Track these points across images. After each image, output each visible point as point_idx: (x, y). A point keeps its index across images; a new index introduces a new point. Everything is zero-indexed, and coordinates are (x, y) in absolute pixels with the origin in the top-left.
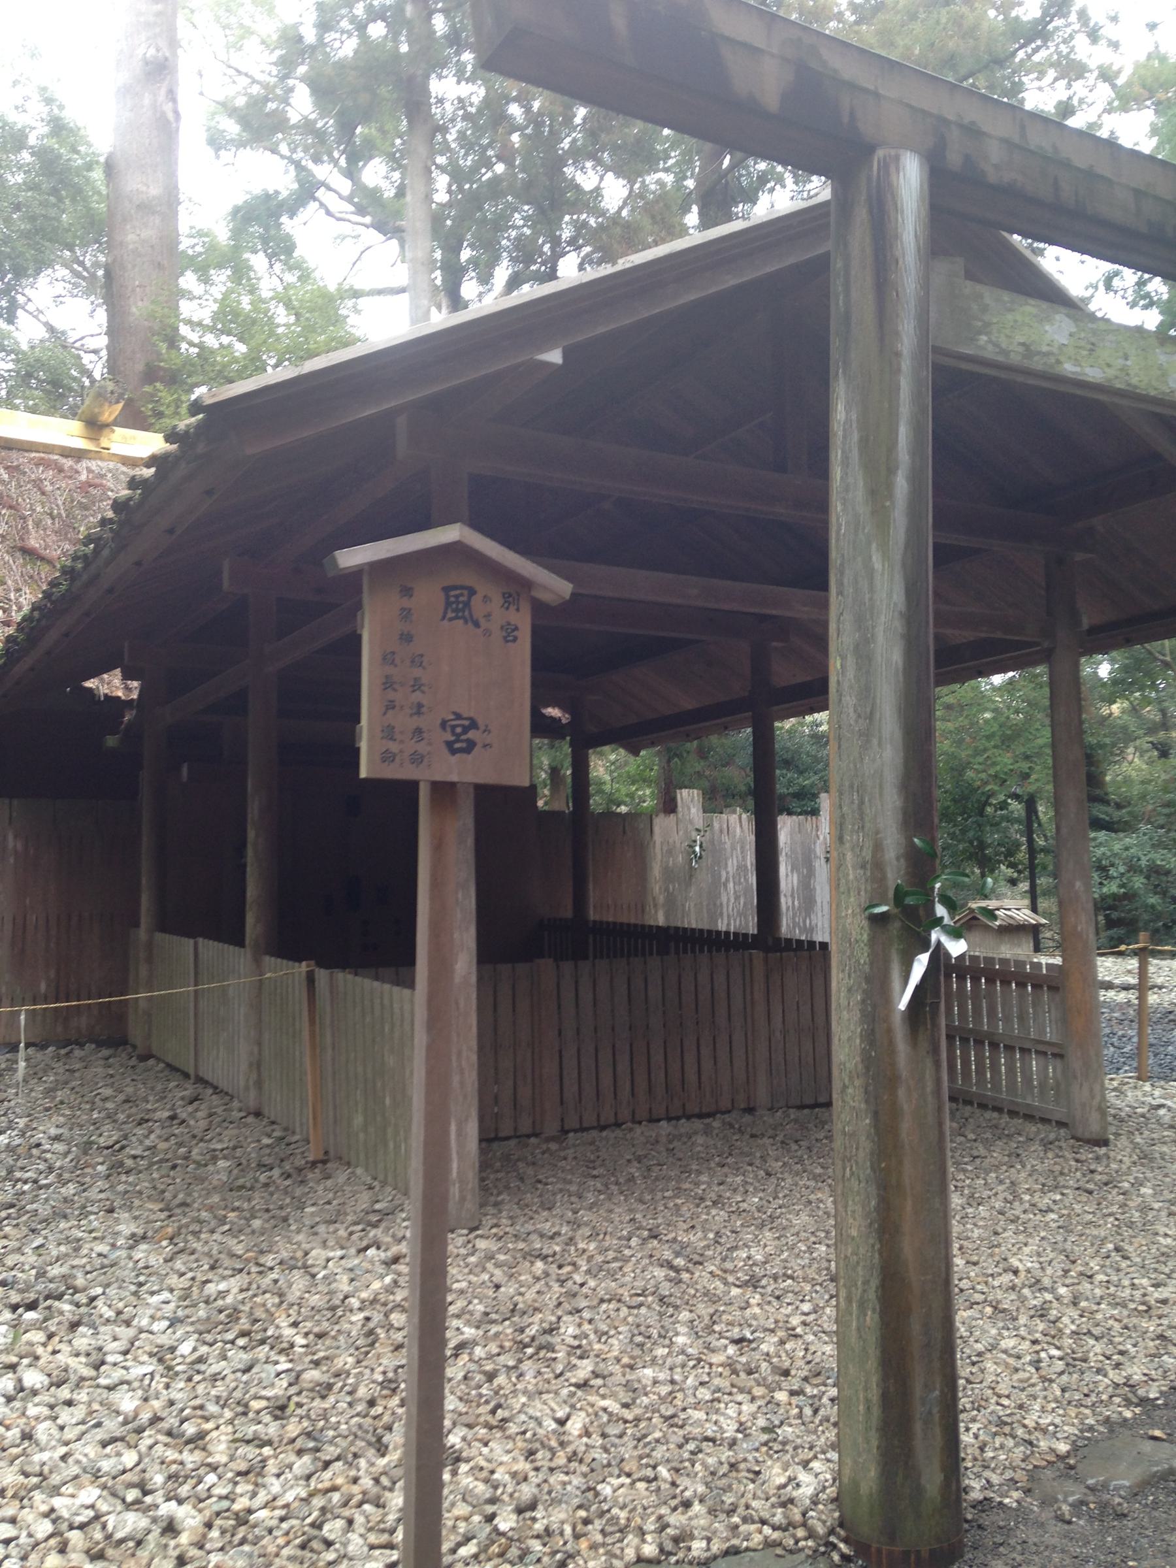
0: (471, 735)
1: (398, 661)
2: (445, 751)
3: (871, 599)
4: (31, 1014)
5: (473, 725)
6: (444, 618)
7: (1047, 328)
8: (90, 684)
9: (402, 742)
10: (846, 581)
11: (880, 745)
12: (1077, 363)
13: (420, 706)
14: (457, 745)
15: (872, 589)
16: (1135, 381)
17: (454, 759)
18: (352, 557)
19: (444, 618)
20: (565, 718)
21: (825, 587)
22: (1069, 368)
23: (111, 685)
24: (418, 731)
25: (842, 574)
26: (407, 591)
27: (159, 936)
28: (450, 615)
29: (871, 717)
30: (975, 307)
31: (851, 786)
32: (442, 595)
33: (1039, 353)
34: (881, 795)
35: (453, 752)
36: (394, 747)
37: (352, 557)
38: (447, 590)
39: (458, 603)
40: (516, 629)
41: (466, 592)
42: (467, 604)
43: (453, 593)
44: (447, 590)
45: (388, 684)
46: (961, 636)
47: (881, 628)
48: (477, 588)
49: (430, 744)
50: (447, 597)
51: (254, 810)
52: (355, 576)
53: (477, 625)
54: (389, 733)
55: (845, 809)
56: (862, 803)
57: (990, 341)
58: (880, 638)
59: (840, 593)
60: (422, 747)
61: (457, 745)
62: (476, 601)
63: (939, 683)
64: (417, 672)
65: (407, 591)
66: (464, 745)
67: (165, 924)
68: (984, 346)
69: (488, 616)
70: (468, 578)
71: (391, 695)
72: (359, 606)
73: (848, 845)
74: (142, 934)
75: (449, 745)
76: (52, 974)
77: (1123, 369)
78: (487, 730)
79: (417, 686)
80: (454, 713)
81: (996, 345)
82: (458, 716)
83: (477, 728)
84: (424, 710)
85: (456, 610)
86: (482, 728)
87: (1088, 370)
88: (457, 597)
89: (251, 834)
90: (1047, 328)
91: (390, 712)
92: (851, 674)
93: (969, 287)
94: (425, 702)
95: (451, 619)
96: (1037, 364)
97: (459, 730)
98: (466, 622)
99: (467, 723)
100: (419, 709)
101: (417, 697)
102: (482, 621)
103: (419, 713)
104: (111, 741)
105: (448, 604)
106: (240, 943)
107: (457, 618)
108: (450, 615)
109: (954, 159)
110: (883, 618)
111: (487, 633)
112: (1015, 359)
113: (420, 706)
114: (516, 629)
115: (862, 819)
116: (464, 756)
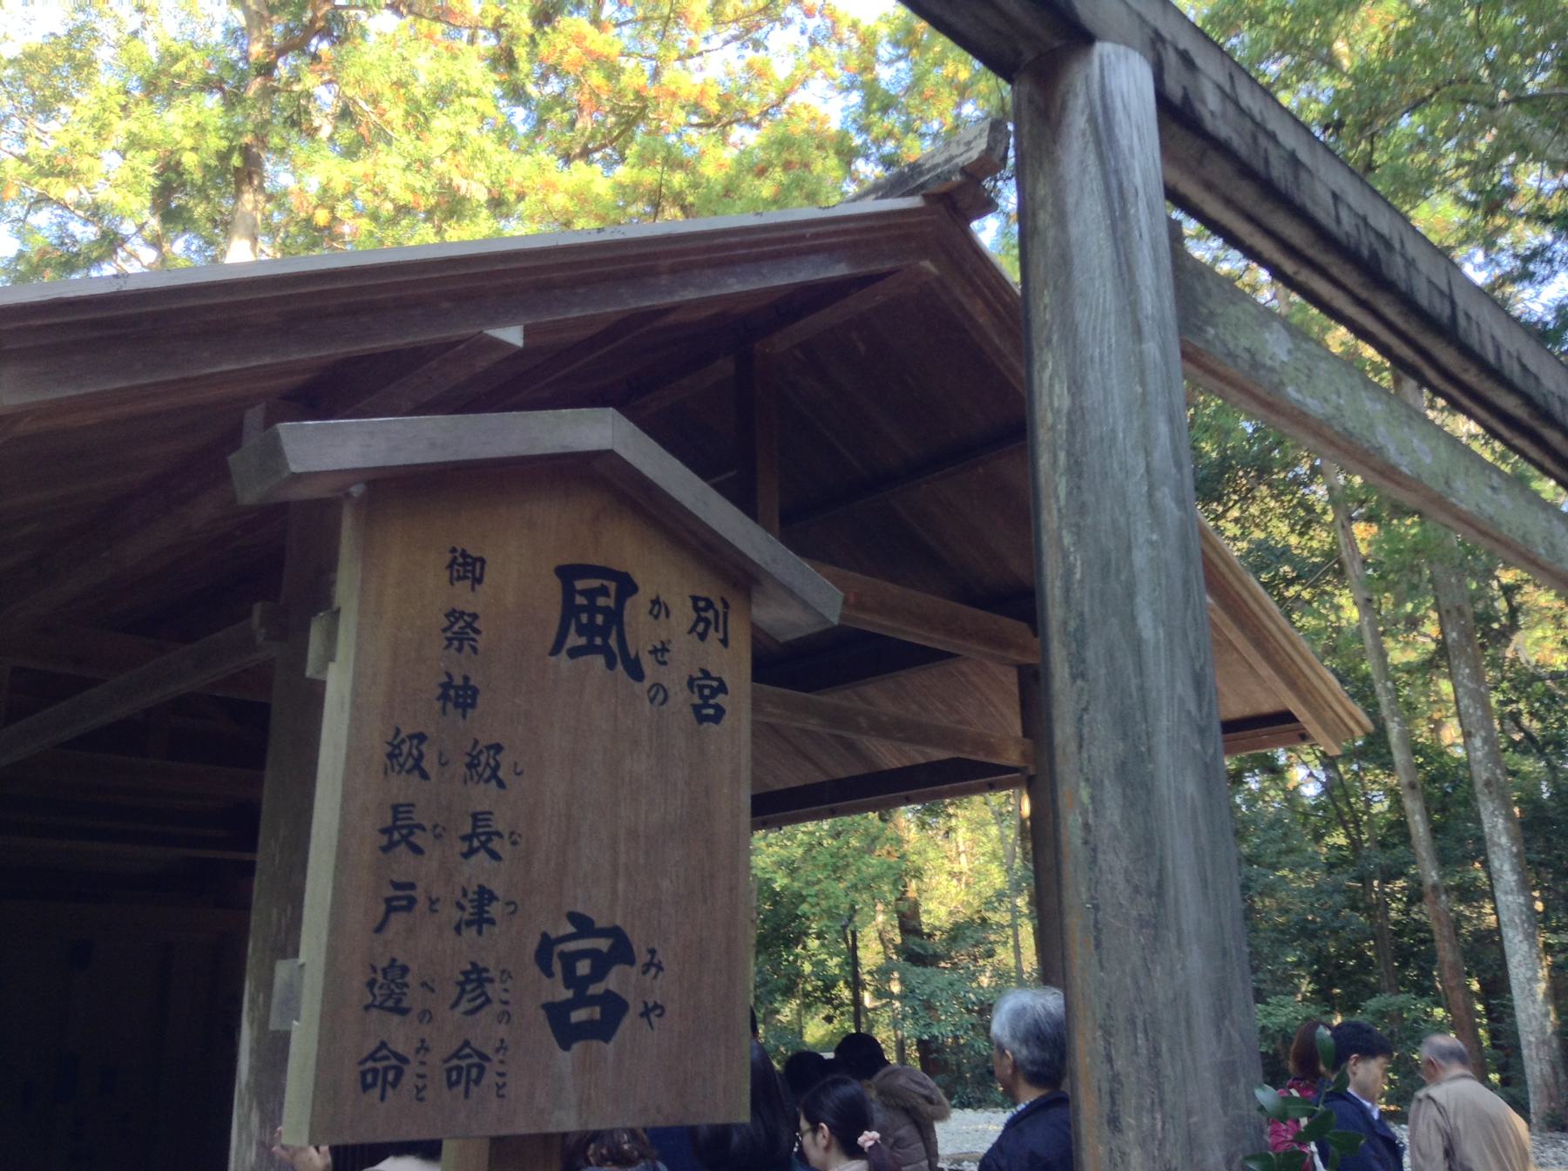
0: (614, 980)
1: (429, 764)
2: (545, 1034)
3: (1141, 688)
5: (622, 950)
6: (556, 650)
7: (1267, 335)
9: (426, 1015)
10: (1090, 655)
11: (1179, 944)
12: (1299, 390)
13: (485, 896)
14: (578, 1016)
15: (1140, 671)
17: (565, 1060)
19: (556, 650)
21: (261, 765)
24: (475, 977)
25: (1082, 643)
28: (574, 640)
29: (1159, 892)
30: (1199, 288)
31: (1132, 1021)
32: (556, 584)
33: (1264, 366)
34: (1190, 1044)
35: (566, 1034)
36: (400, 1035)
38: (568, 574)
39: (592, 609)
40: (722, 688)
41: (612, 586)
42: (615, 617)
43: (580, 585)
44: (568, 574)
45: (400, 830)
46: (790, 777)
47: (1164, 737)
48: (638, 578)
49: (505, 1017)
50: (569, 592)
53: (635, 670)
54: (389, 988)
55: (1119, 1064)
56: (1156, 1053)
57: (1217, 336)
58: (1164, 756)
59: (1078, 674)
60: (485, 1031)
61: (578, 1016)
62: (636, 611)
63: (756, 826)
64: (482, 796)
66: (596, 1012)
69: (660, 651)
70: (625, 547)
71: (404, 865)
72: (319, 598)
73: (1131, 1135)
75: (556, 1014)
78: (652, 965)
79: (480, 836)
80: (574, 918)
81: (1224, 344)
82: (584, 926)
83: (630, 960)
84: (495, 910)
85: (586, 630)
86: (642, 957)
87: (1309, 401)
88: (591, 594)
90: (1267, 335)
91: (398, 921)
92: (1113, 812)
94: (497, 887)
95: (575, 653)
97: (583, 968)
98: (611, 664)
99: (603, 944)
100: (479, 908)
101: (478, 870)
102: (648, 663)
103: (481, 920)
105: (569, 611)
107: (589, 649)
108: (574, 640)
110: (1164, 723)
111: (660, 693)
113: (485, 896)
114: (722, 688)
115: (1159, 1086)
116: (595, 1044)
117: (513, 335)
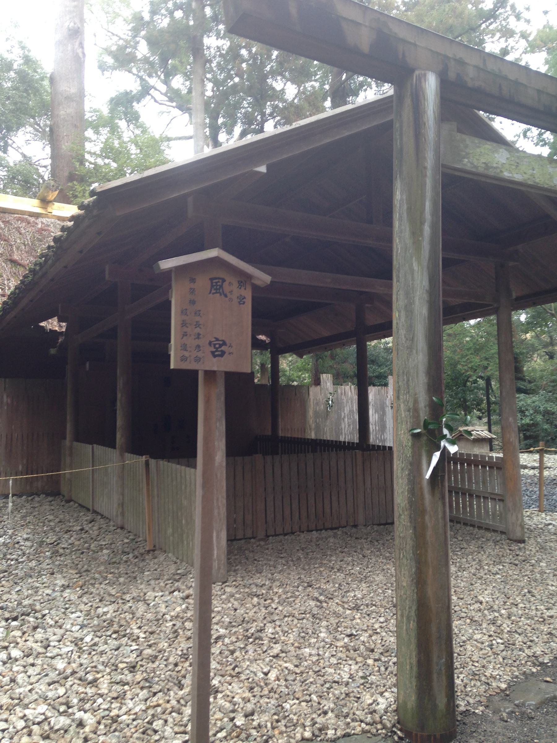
0: (223, 348)
1: (188, 313)
2: (211, 356)
3: (412, 284)
4: (15, 481)
5: (224, 343)
6: (210, 293)
7: (496, 155)
8: (42, 324)
9: (190, 351)
10: (400, 275)
11: (417, 353)
12: (510, 172)
13: (199, 334)
14: (216, 353)
15: (413, 279)
16: (537, 180)
17: (215, 360)
18: (167, 264)
19: (210, 293)
20: (268, 340)
21: (391, 278)
22: (506, 174)
23: (53, 324)
24: (198, 346)
25: (399, 272)
26: (193, 280)
27: (75, 444)
28: (213, 291)
29: (412, 340)
30: (462, 145)
31: (403, 373)
32: (209, 282)
33: (492, 167)
35: (215, 356)
36: (186, 354)
37: (167, 264)
38: (211, 279)
39: (217, 286)
40: (245, 298)
41: (221, 281)
42: (221, 286)
43: (214, 281)
44: (211, 279)
45: (184, 324)
46: (455, 301)
47: (417, 298)
48: (226, 278)
49: (204, 353)
50: (212, 283)
51: (120, 384)
52: (168, 273)
53: (226, 296)
54: (184, 347)
55: (400, 383)
56: (408, 380)
57: (469, 162)
58: (417, 302)
59: (398, 281)
60: (200, 354)
61: (216, 353)
62: (226, 285)
63: (445, 324)
64: (198, 319)
65: (193, 280)
66: (220, 353)
67: (78, 438)
68: (466, 164)
69: (231, 292)
70: (222, 274)
71: (185, 329)
72: (170, 287)
73: (401, 400)
74: (67, 442)
75: (213, 353)
76: (25, 461)
77: (532, 175)
78: (230, 346)
79: (197, 325)
80: (215, 338)
81: (472, 163)
82: (217, 339)
83: (226, 345)
84: (201, 336)
85: (216, 289)
86: (228, 345)
87: (515, 176)
88: (216, 283)
89: (119, 395)
90: (496, 155)
91: (185, 337)
92: (403, 319)
93: (459, 136)
94: (201, 333)
95: (213, 294)
96: (491, 173)
97: (217, 346)
98: (221, 295)
99: (221, 342)
100: (198, 336)
101: (197, 330)
102: (228, 294)
103: (198, 338)
104: (53, 351)
105: (212, 286)
106: (114, 447)
107: (216, 293)
108: (213, 291)
109: (452, 75)
110: (418, 293)
111: (231, 300)
112: (481, 170)
113: (199, 334)
114: (245, 298)
115: (408, 388)
116: (220, 358)
117: (263, 169)
